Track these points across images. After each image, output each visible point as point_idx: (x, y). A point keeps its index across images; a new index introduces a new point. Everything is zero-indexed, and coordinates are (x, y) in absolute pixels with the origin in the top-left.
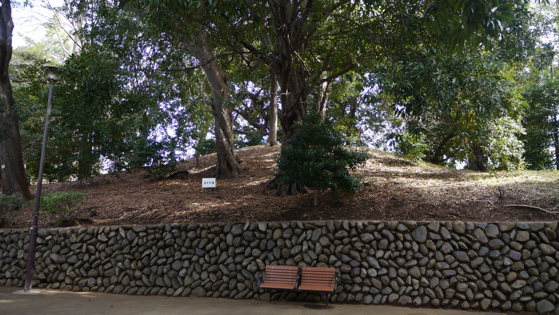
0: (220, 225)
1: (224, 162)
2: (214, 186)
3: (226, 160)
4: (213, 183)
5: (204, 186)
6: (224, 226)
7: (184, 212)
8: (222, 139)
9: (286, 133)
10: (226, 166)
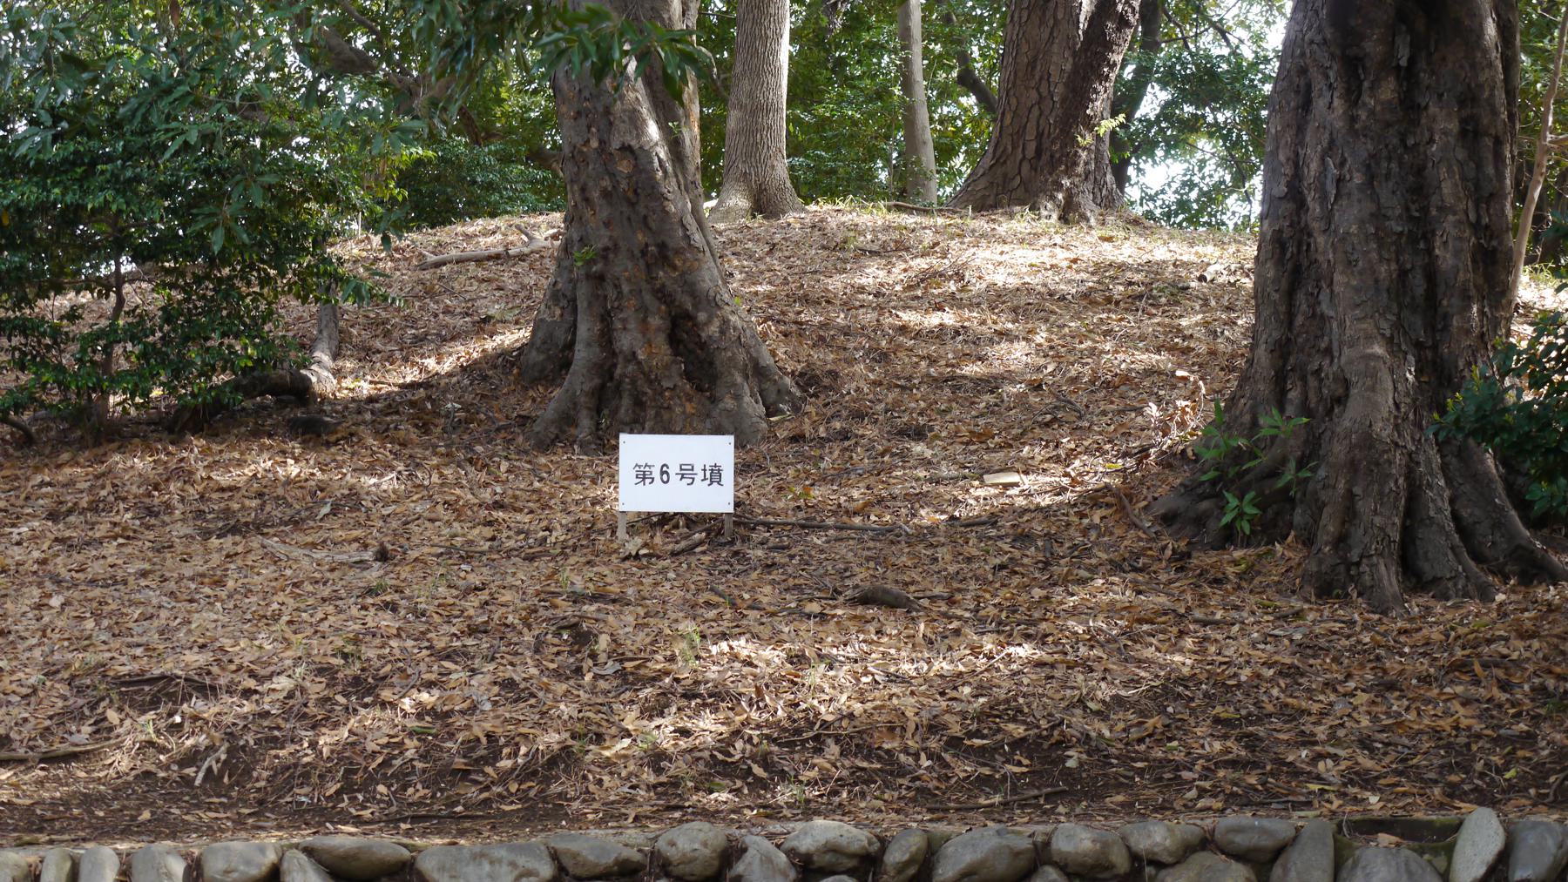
0: (1241, 840)
1: (644, 311)
2: (719, 500)
3: (662, 295)
4: (643, 476)
5: (633, 497)
6: (1279, 851)
7: (708, 726)
8: (637, 124)
9: (1353, 96)
10: (663, 350)
